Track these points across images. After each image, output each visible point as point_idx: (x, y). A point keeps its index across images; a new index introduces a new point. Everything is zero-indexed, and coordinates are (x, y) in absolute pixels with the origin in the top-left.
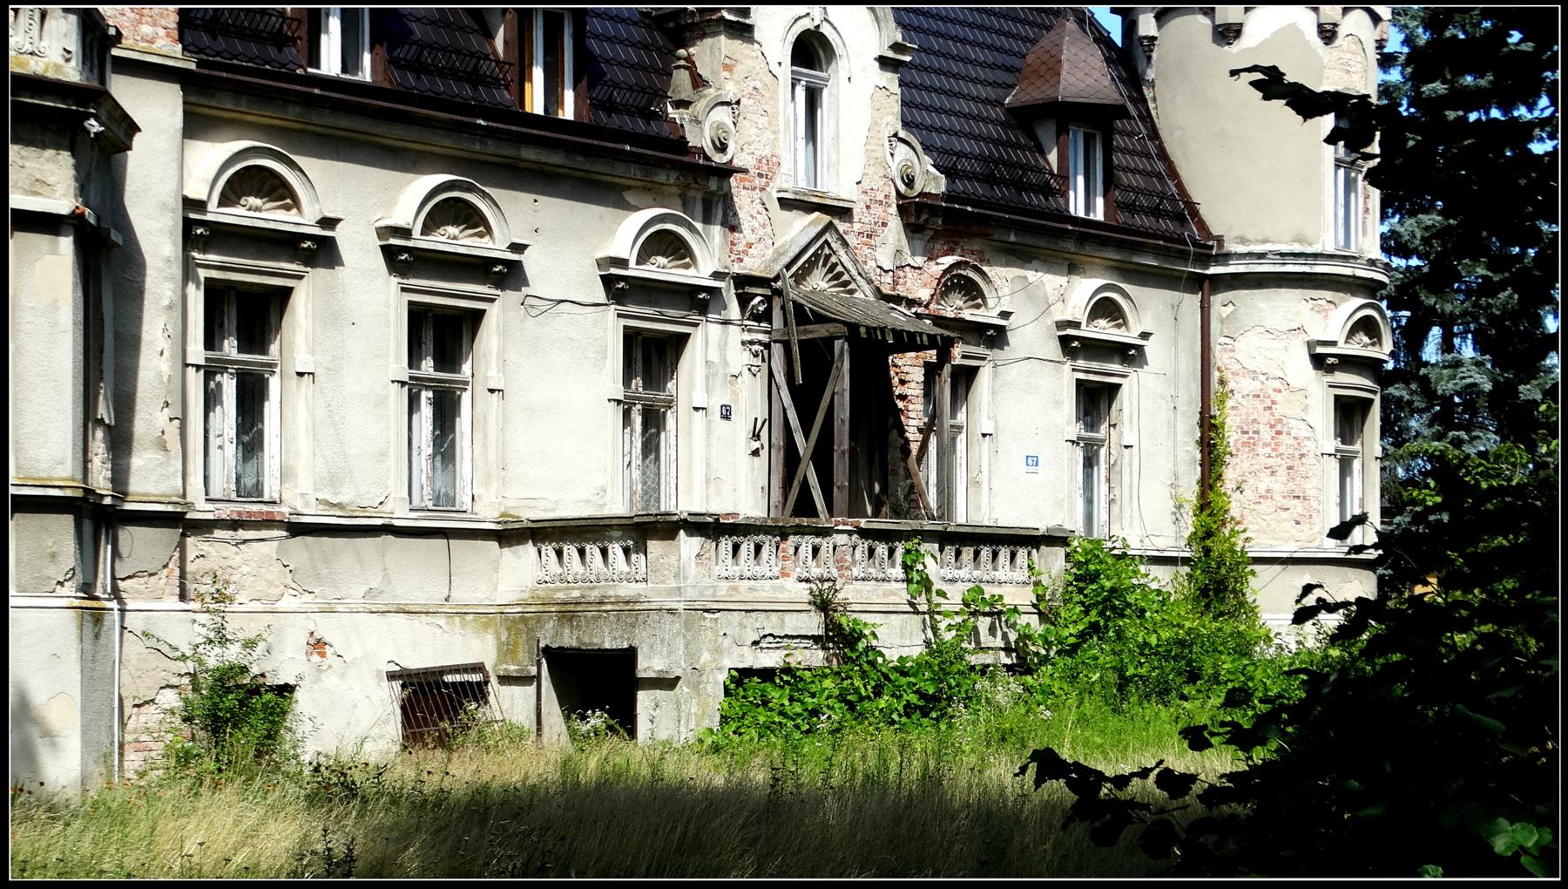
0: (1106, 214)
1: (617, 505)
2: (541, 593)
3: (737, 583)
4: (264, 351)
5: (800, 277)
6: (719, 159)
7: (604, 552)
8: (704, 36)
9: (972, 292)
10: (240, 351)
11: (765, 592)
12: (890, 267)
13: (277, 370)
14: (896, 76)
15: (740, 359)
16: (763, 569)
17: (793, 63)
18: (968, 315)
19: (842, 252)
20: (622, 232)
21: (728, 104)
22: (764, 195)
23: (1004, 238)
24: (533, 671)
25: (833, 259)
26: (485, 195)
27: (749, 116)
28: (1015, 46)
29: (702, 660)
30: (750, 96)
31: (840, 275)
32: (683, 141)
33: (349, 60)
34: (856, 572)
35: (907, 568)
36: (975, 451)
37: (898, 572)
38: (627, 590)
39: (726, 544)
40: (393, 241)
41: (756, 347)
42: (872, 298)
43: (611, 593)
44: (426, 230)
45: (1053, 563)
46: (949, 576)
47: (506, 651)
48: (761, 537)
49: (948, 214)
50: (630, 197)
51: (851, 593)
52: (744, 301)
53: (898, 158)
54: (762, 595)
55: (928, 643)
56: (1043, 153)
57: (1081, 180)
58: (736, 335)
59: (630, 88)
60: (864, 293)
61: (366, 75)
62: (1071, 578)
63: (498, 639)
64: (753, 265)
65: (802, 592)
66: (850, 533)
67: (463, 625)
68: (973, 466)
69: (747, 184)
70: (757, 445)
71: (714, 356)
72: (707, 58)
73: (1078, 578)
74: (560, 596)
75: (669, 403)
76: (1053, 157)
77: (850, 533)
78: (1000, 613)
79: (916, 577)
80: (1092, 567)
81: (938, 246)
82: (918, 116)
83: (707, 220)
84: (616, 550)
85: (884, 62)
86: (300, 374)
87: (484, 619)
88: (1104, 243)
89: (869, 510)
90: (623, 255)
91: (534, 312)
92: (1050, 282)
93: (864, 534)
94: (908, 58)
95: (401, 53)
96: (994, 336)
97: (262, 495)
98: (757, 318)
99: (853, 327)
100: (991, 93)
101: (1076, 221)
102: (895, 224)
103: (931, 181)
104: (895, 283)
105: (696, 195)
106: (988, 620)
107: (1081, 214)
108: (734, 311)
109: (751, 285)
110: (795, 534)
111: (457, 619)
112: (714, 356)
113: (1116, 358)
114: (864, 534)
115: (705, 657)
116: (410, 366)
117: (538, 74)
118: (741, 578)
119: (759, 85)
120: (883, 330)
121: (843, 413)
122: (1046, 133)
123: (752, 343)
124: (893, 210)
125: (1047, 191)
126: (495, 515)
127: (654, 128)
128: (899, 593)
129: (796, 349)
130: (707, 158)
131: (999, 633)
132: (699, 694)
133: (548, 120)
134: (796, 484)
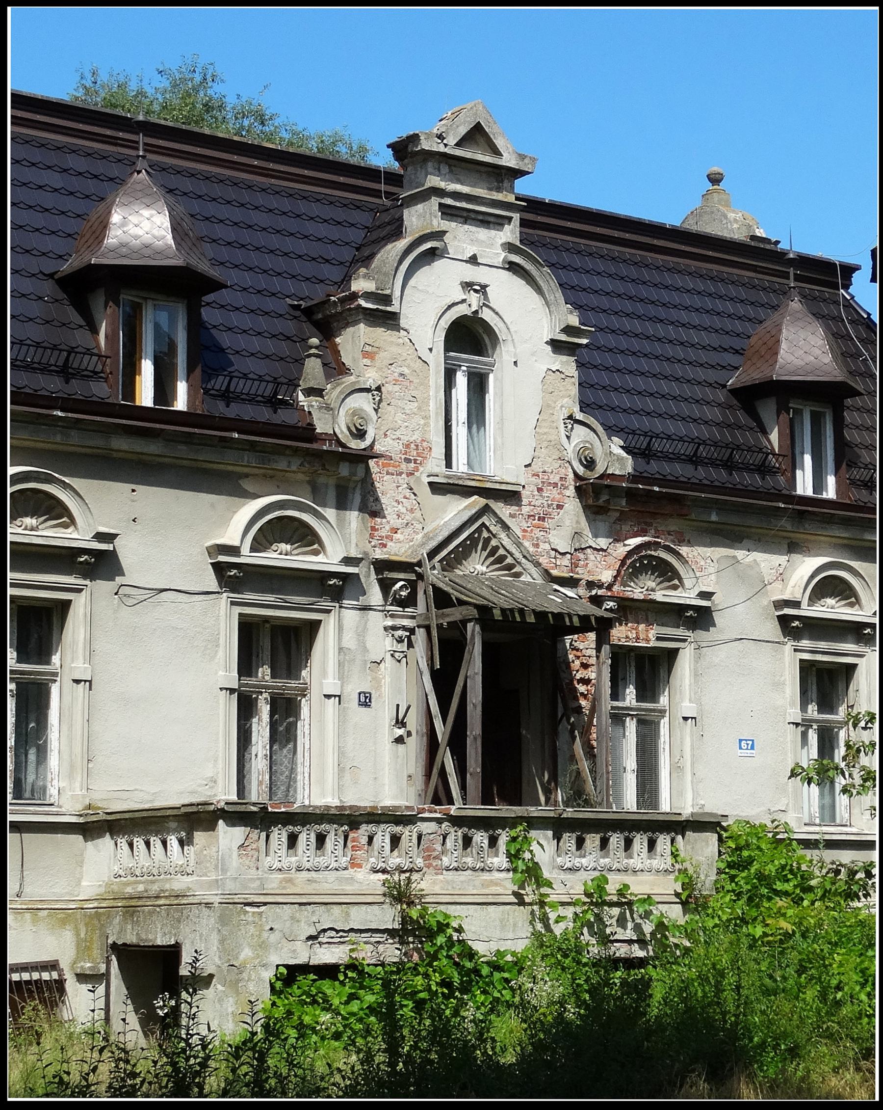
0: (838, 492)
1: (224, 793)
2: (115, 888)
3: (293, 874)
4: (48, 663)
5: (449, 564)
6: (356, 445)
7: (164, 843)
8: (348, 325)
9: (667, 574)
10: (820, 711)
11: (328, 883)
12: (559, 550)
13: (58, 679)
14: (573, 359)
15: (382, 644)
16: (322, 861)
17: (447, 349)
18: (659, 596)
19: (503, 535)
20: (235, 521)
21: (368, 390)
22: (412, 480)
23: (704, 517)
24: (103, 968)
25: (494, 543)
26: (66, 486)
27: (393, 402)
28: (739, 326)
29: (242, 957)
30: (396, 382)
31: (502, 558)
32: (311, 427)
33: (819, 483)
34: (446, 861)
35: (513, 857)
36: (677, 733)
37: (500, 860)
38: (179, 883)
39: (279, 836)
40: (222, 558)
41: (400, 633)
42: (540, 581)
43: (167, 886)
44: (812, 600)
45: (703, 851)
46: (568, 865)
47: (83, 948)
48: (324, 827)
49: (630, 494)
50: (247, 485)
51: (428, 884)
52: (385, 586)
53: (575, 440)
54: (326, 887)
55: (536, 935)
56: (765, 432)
57: (808, 459)
58: (377, 621)
59: (681, 439)
60: (531, 576)
61: (830, 493)
62: (722, 866)
63: (78, 935)
64: (399, 549)
65: (372, 883)
66: (439, 821)
67: (35, 921)
68: (677, 753)
69: (391, 469)
70: (400, 732)
71: (349, 641)
72: (349, 347)
73: (730, 865)
74: (129, 890)
75: (303, 692)
76: (774, 437)
77: (439, 821)
78: (630, 904)
79: (521, 866)
80: (745, 853)
81: (626, 528)
82: (602, 397)
83: (342, 505)
84: (173, 841)
85: (556, 346)
86: (685, 719)
87: (61, 915)
88: (828, 520)
89: (542, 799)
90: (798, 596)
91: (131, 602)
92: (766, 562)
93: (457, 821)
94: (585, 341)
95: (220, 383)
96: (699, 618)
97: (834, 821)
98: (403, 603)
99: (484, 611)
100: (712, 376)
101: (804, 500)
102: (573, 506)
103: (614, 457)
104: (574, 565)
105: (327, 481)
106: (616, 911)
107: (809, 492)
108: (375, 596)
109: (390, 571)
110: (368, 822)
111: (28, 916)
112: (349, 641)
113: (849, 637)
114: (457, 821)
115: (246, 953)
116: (241, 673)
117: (147, 368)
118: (299, 869)
119: (406, 371)
120: (521, 611)
121: (476, 696)
122: (767, 410)
123: (394, 628)
124: (571, 491)
125: (764, 469)
126: (79, 807)
127: (283, 416)
128: (504, 883)
129: (435, 633)
130: (343, 446)
131: (630, 925)
132: (238, 993)
133: (161, 413)
134: (435, 771)
